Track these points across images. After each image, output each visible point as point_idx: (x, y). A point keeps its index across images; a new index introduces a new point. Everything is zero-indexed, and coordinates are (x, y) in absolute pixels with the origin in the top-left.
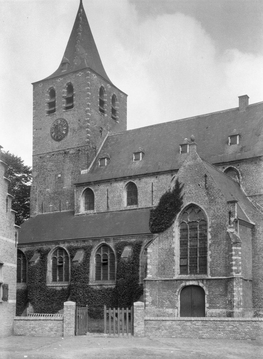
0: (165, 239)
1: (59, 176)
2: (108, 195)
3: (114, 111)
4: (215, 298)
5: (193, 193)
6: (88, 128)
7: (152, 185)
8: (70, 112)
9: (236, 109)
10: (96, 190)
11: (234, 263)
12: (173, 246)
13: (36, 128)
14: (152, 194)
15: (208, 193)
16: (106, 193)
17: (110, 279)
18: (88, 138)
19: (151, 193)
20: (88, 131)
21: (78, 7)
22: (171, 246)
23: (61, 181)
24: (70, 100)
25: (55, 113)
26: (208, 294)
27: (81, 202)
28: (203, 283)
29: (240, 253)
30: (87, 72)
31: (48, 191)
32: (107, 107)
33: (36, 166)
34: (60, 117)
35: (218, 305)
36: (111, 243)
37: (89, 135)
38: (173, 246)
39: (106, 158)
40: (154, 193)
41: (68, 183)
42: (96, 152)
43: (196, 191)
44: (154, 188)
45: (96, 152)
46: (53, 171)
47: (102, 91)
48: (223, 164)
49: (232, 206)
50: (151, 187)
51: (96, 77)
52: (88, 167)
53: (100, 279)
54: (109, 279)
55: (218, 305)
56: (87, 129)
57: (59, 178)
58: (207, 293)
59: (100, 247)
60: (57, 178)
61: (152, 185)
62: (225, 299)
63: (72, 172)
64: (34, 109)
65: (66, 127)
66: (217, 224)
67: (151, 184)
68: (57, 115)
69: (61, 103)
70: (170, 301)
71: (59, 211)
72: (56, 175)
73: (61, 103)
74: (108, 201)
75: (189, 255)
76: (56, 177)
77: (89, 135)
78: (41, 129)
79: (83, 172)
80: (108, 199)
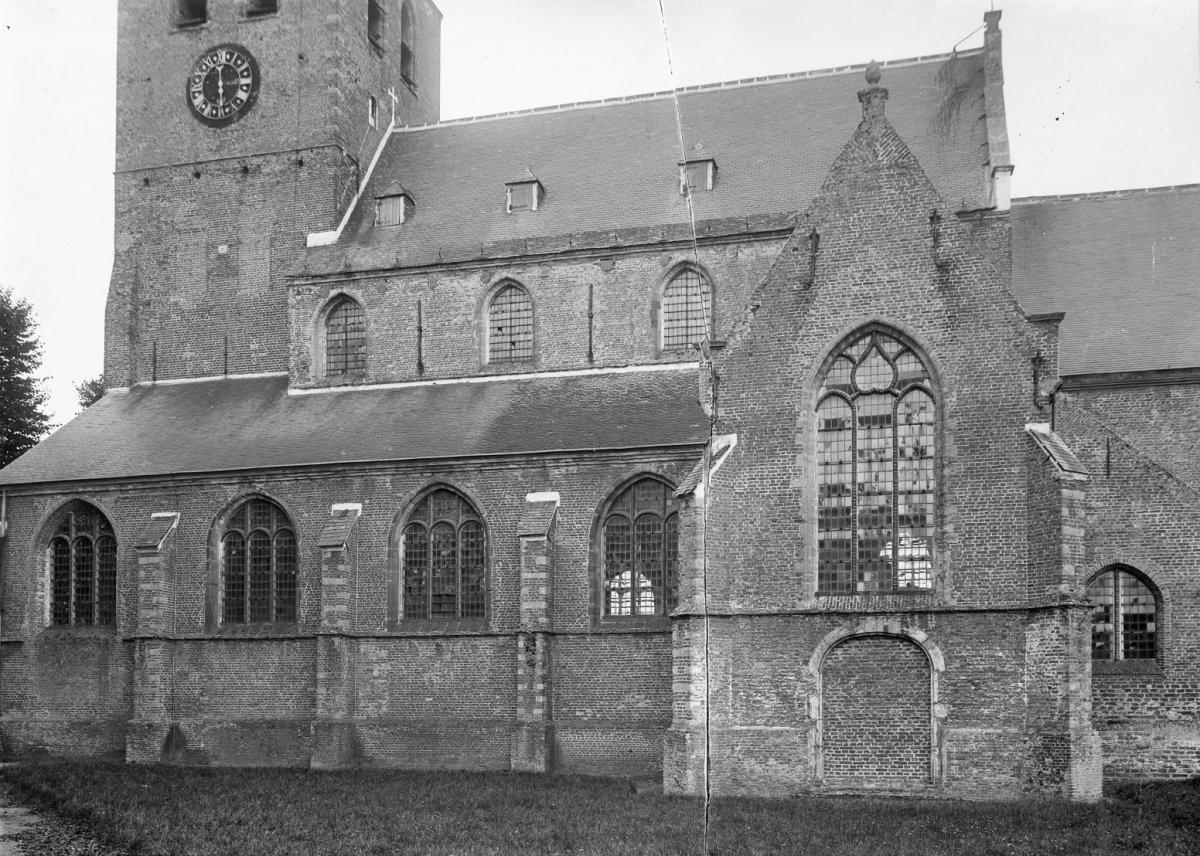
0: (759, 455)
1: (223, 249)
2: (420, 322)
3: (406, 55)
4: (974, 684)
5: (880, 281)
7: (591, 295)
8: (266, 26)
10: (372, 304)
12: (795, 483)
13: (130, 79)
14: (591, 323)
16: (415, 314)
17: (101, 622)
18: (334, 120)
19: (587, 319)
22: (785, 484)
23: (226, 268)
25: (204, 25)
26: (942, 669)
27: (312, 338)
28: (924, 626)
31: (176, 304)
32: (390, 40)
33: (129, 211)
34: (227, 40)
35: (986, 712)
36: (469, 485)
38: (795, 483)
39: (403, 195)
40: (598, 323)
41: (256, 271)
42: (358, 176)
43: (894, 274)
44: (596, 302)
45: (358, 176)
46: (195, 231)
49: (1045, 335)
50: (585, 298)
52: (337, 222)
53: (241, 619)
54: (96, 622)
55: (986, 712)
56: (331, 90)
57: (220, 257)
58: (939, 662)
59: (426, 499)
60: (213, 256)
61: (591, 295)
62: (1016, 687)
63: (273, 240)
65: (248, 76)
66: (983, 402)
67: (586, 289)
70: (784, 698)
71: (220, 378)
72: (211, 247)
74: (420, 341)
75: (460, 563)
78: (149, 79)
79: (315, 239)
80: (420, 337)
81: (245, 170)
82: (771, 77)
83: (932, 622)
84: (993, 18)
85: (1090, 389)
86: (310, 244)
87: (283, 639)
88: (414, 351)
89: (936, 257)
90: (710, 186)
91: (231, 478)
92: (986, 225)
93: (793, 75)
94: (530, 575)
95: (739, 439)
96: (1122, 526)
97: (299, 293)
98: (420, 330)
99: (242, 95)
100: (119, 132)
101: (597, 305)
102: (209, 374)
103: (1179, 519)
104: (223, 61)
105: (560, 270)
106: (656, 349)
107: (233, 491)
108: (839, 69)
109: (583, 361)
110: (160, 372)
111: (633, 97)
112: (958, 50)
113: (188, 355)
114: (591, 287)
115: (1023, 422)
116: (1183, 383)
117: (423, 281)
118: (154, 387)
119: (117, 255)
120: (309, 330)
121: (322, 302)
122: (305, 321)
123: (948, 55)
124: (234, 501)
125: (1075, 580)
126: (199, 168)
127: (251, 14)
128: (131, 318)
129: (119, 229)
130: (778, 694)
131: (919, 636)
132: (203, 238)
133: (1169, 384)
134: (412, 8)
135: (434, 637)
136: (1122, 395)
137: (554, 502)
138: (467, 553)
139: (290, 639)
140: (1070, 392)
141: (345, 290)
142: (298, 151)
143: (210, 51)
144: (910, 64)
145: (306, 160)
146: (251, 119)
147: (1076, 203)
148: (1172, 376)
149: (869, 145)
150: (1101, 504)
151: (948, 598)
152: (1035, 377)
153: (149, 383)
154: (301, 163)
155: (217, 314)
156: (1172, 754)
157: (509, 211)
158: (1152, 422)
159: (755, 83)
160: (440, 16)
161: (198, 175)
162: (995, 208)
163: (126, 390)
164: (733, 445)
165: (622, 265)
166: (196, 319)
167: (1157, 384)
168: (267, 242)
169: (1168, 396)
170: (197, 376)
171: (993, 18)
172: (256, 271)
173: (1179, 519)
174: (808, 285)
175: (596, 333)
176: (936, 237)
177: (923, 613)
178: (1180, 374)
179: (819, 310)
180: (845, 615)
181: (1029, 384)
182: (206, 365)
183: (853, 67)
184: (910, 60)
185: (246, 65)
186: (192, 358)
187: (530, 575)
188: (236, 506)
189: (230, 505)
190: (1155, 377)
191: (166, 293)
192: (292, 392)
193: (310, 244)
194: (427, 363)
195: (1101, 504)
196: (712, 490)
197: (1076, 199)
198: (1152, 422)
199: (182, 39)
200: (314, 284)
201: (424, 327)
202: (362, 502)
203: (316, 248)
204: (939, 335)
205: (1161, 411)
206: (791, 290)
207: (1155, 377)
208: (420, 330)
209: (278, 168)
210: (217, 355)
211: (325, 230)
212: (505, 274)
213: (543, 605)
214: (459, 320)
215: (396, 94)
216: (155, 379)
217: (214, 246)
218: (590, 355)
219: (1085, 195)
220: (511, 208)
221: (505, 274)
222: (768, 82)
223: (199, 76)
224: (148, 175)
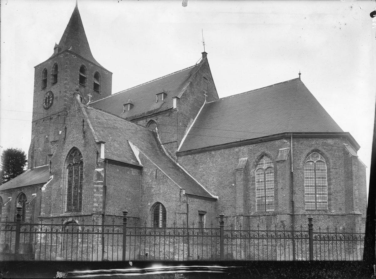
6: (65, 97)
9: (67, 35)
11: (95, 200)
15: (84, 137)
18: (65, 105)
20: (65, 100)
21: (213, 77)
24: (55, 76)
29: (95, 190)
30: (66, 53)
37: (66, 103)
47: (82, 70)
48: (142, 117)
51: (76, 57)
64: (34, 87)
66: (89, 164)
68: (48, 89)
69: (50, 80)
73: (50, 80)
76: (45, 138)
77: (66, 103)
82: (158, 79)
84: (204, 54)
85: (194, 153)
90: (129, 110)
91: (18, 189)
92: (173, 113)
93: (162, 77)
96: (158, 192)
97: (53, 145)
99: (51, 102)
104: (48, 95)
107: (19, 192)
108: (172, 74)
111: (132, 88)
112: (197, 64)
115: (95, 169)
116: (214, 150)
123: (194, 66)
124: (19, 194)
125: (98, 207)
127: (54, 83)
128: (32, 154)
132: (44, 135)
133: (211, 150)
134: (99, 74)
136: (201, 154)
140: (190, 155)
144: (187, 69)
146: (52, 107)
147: (223, 100)
148: (211, 148)
150: (155, 186)
154: (59, 115)
156: (167, 253)
158: (208, 161)
159: (155, 80)
162: (173, 108)
163: (30, 169)
164: (52, 178)
167: (208, 151)
168: (53, 134)
169: (211, 154)
170: (42, 165)
171: (204, 54)
174: (65, 139)
176: (83, 125)
177: (78, 216)
178: (213, 148)
179: (66, 145)
180: (66, 217)
183: (175, 73)
184: (186, 69)
188: (20, 195)
189: (19, 195)
190: (207, 149)
191: (38, 148)
195: (155, 186)
196: (47, 189)
197: (223, 99)
198: (208, 161)
199: (43, 91)
200: (55, 143)
202: (36, 193)
204: (83, 149)
205: (209, 158)
206: (62, 141)
207: (207, 149)
209: (56, 117)
219: (225, 98)
222: (158, 80)
224: (37, 122)
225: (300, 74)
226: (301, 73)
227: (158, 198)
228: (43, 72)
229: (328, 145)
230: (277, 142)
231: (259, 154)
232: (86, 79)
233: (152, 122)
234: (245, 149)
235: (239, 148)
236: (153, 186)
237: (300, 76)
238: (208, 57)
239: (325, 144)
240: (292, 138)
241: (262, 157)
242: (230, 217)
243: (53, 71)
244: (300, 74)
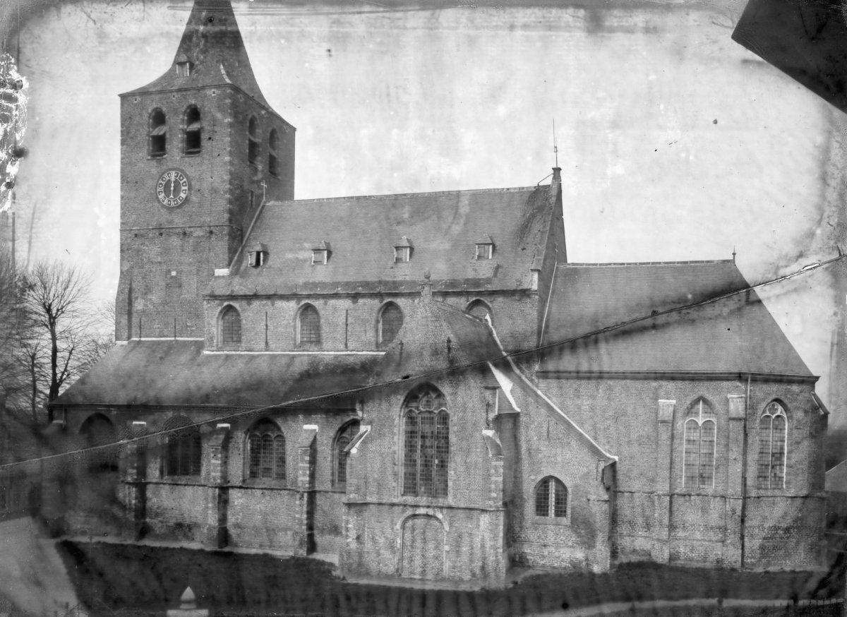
1: (174, 273)
28: (442, 512)
44: (349, 319)
57: (172, 277)
61: (347, 314)
65: (186, 186)
67: (345, 312)
71: (173, 339)
74: (266, 332)
80: (267, 329)
81: (185, 234)
83: (445, 511)
84: (557, 171)
86: (216, 274)
87: (194, 485)
88: (264, 336)
89: (449, 357)
94: (302, 465)
95: (372, 428)
98: (267, 326)
100: (122, 209)
101: (350, 320)
102: (167, 336)
103: (576, 458)
105: (332, 302)
106: (377, 343)
109: (342, 347)
110: (144, 333)
112: (540, 184)
113: (156, 326)
114: (347, 311)
117: (269, 303)
118: (139, 342)
119: (122, 272)
120: (214, 322)
121: (220, 308)
122: (212, 317)
126: (162, 231)
129: (122, 259)
130: (385, 537)
131: (440, 516)
135: (262, 489)
137: (315, 430)
138: (278, 449)
139: (197, 485)
141: (231, 303)
142: (210, 227)
143: (167, 170)
145: (214, 231)
149: (423, 306)
150: (545, 449)
151: (451, 501)
152: (487, 412)
153: (137, 339)
155: (170, 306)
157: (313, 263)
160: (294, 129)
161: (161, 234)
163: (125, 343)
165: (361, 301)
166: (160, 308)
168: (195, 271)
171: (557, 171)
172: (191, 288)
173: (576, 458)
175: (349, 333)
181: (484, 415)
182: (166, 333)
185: (185, 180)
186: (158, 328)
187: (302, 465)
192: (206, 352)
193: (216, 274)
194: (270, 342)
195: (545, 449)
201: (269, 325)
203: (219, 277)
208: (267, 326)
210: (171, 328)
211: (223, 268)
212: (307, 301)
213: (308, 479)
214: (285, 322)
215: (263, 186)
216: (140, 337)
217: (169, 271)
218: (346, 344)
220: (314, 262)
221: (307, 301)
223: (161, 184)
225: (734, 254)
226: (736, 252)
227: (551, 470)
228: (150, 114)
229: (793, 393)
230: (725, 384)
231: (693, 397)
232: (258, 147)
233: (477, 303)
234: (670, 386)
235: (660, 381)
236: (542, 448)
237: (734, 258)
238: (564, 176)
239: (788, 391)
240: (749, 381)
241: (697, 402)
242: (639, 492)
243: (183, 120)
244: (734, 254)
